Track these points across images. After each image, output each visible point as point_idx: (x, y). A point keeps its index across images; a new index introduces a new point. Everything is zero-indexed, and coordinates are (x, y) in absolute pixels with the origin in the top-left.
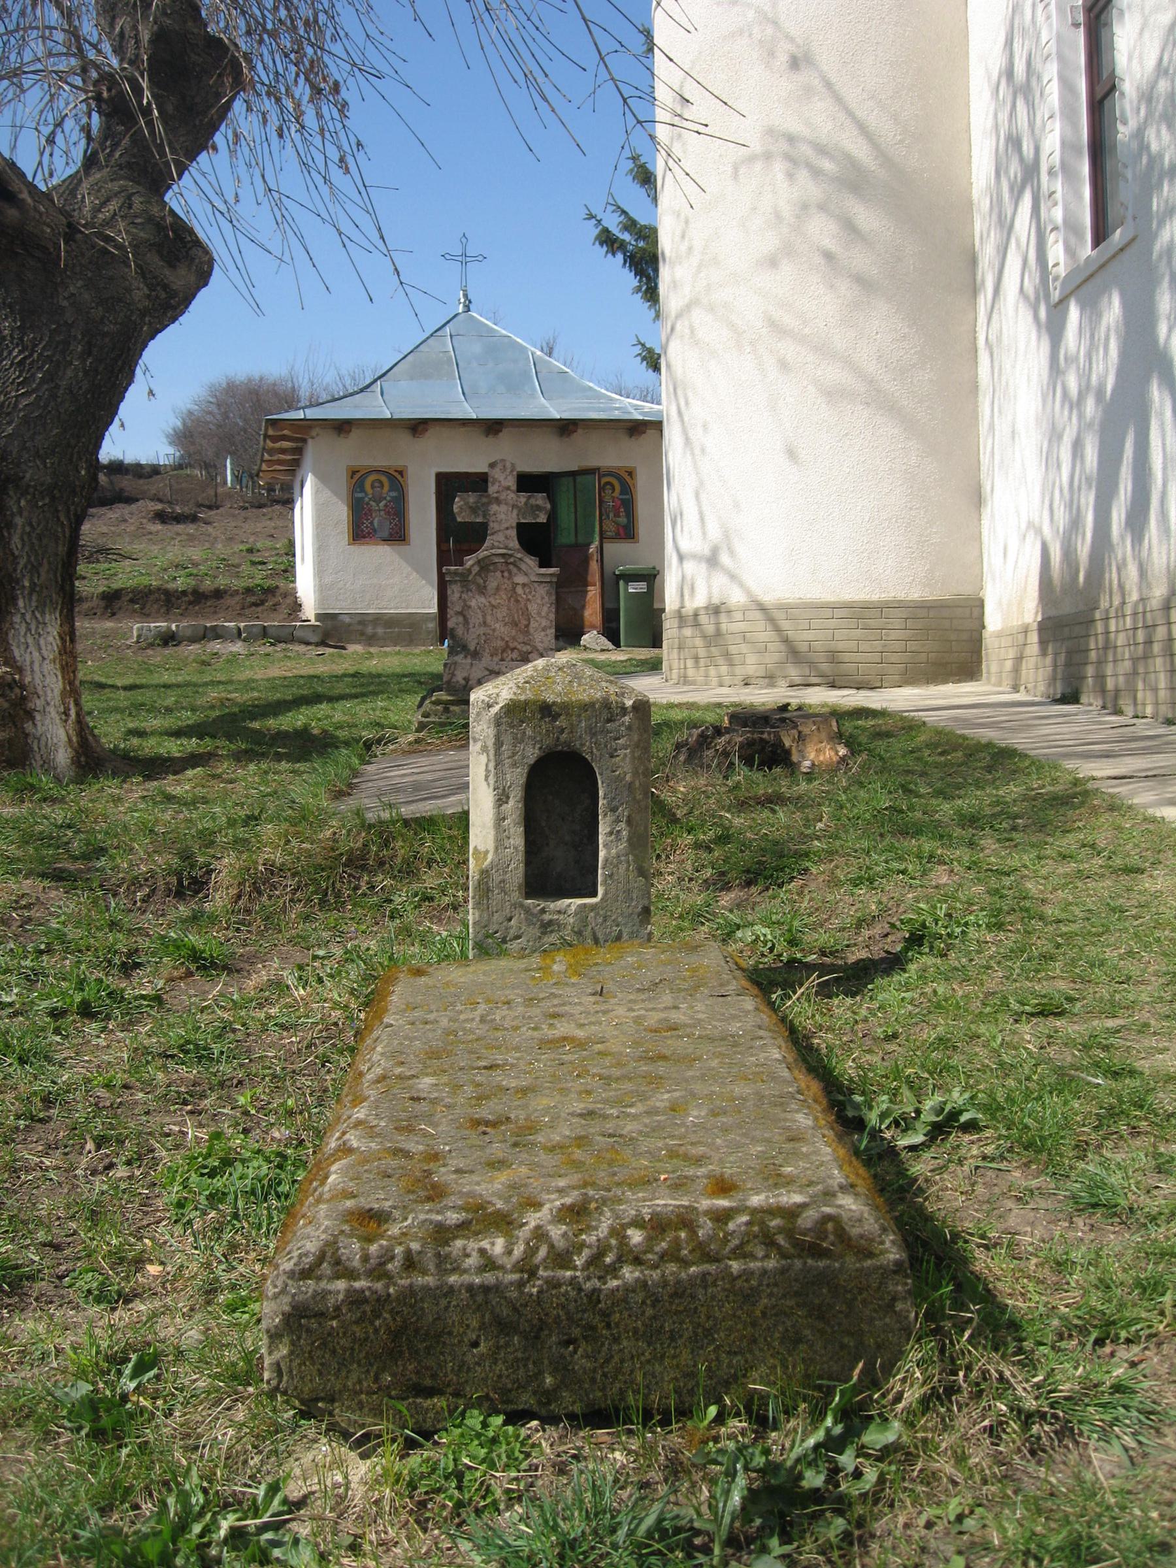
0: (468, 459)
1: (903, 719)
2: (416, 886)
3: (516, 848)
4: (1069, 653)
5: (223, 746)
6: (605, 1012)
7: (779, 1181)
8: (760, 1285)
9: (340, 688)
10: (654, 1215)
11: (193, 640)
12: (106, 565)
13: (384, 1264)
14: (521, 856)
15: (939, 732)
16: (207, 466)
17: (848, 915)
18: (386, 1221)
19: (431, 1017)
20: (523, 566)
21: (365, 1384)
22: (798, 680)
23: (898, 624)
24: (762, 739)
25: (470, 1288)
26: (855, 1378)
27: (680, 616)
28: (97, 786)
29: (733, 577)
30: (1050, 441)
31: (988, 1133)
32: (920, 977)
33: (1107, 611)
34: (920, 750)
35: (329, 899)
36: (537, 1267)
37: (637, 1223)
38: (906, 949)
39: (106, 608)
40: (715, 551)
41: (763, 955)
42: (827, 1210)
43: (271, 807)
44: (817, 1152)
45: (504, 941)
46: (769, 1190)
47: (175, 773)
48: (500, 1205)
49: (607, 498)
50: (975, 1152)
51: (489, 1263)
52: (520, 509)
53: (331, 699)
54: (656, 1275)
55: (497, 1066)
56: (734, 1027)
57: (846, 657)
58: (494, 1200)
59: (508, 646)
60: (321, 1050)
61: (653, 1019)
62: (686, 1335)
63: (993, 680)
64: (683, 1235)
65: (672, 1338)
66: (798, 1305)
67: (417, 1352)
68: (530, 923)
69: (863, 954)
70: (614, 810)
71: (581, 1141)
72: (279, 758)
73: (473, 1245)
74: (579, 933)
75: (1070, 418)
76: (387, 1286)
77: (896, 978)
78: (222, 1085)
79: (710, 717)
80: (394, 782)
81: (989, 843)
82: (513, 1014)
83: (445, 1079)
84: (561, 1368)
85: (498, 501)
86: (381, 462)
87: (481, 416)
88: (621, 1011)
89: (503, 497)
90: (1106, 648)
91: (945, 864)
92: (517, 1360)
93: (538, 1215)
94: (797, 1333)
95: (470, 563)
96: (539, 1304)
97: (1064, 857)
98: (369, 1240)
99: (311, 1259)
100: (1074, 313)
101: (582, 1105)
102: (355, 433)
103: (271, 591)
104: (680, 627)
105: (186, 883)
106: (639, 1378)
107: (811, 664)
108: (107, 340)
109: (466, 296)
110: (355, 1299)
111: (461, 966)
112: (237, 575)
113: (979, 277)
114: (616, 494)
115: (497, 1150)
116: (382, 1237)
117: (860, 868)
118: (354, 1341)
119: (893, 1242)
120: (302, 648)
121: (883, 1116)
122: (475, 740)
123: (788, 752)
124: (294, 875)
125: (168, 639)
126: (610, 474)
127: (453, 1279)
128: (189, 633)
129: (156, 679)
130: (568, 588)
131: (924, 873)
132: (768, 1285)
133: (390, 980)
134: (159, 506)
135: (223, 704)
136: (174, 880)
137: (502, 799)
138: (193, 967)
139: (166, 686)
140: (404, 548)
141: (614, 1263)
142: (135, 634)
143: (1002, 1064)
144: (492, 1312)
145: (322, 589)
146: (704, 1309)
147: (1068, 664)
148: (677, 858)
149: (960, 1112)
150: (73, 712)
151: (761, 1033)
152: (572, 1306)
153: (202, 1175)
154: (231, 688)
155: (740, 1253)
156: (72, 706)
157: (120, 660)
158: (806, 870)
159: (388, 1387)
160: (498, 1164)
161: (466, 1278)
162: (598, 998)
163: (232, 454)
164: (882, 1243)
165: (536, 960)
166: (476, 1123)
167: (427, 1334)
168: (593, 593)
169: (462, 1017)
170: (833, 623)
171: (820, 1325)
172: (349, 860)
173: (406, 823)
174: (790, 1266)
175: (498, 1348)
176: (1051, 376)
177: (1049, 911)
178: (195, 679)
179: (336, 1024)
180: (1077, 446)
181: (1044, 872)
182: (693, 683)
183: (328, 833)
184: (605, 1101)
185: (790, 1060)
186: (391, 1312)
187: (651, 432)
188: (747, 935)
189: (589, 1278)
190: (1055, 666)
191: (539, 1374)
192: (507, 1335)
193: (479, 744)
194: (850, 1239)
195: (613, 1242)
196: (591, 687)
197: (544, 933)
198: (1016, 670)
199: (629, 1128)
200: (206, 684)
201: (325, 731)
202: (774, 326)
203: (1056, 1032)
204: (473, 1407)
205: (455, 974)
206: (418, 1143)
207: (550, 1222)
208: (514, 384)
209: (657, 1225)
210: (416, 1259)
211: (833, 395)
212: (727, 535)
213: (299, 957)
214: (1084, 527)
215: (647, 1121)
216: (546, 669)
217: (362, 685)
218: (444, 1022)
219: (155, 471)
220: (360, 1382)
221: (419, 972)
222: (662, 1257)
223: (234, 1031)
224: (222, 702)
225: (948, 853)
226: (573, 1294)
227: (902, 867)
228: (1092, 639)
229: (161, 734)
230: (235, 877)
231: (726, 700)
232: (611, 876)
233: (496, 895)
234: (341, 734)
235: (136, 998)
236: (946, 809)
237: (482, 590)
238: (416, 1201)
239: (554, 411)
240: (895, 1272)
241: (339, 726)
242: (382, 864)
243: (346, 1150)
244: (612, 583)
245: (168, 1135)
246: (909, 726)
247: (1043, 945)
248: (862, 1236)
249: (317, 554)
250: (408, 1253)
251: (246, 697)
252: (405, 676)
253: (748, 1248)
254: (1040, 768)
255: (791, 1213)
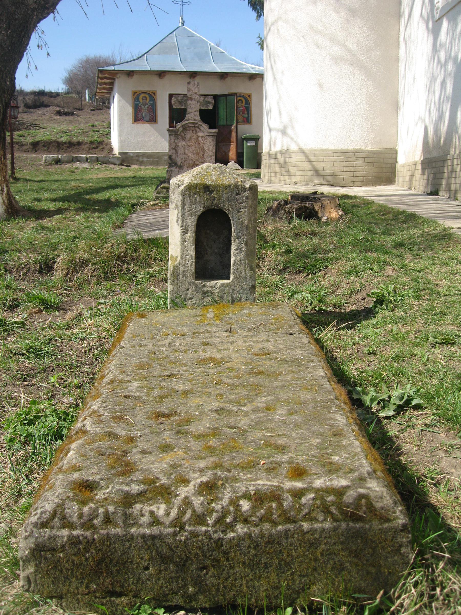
0: (180, 88)
1: (363, 199)
2: (148, 270)
3: (191, 256)
4: (435, 174)
5: (73, 205)
6: (232, 342)
7: (332, 469)
8: (320, 537)
9: (128, 183)
10: (257, 491)
11: (68, 162)
12: (33, 131)
13: (92, 519)
14: (193, 259)
15: (381, 206)
16: (78, 93)
17: (346, 288)
18: (96, 488)
19: (143, 343)
20: (202, 129)
21: (81, 589)
22: (317, 183)
23: (361, 160)
24: (305, 207)
25: (144, 536)
26: (378, 600)
27: (269, 155)
28: (15, 222)
29: (292, 139)
30: (431, 81)
31: (426, 411)
32: (383, 322)
33: (453, 156)
34: (373, 213)
35: (108, 276)
36: (185, 524)
37: (247, 496)
38: (375, 307)
39: (33, 149)
40: (285, 128)
41: (307, 306)
42: (362, 491)
43: (85, 233)
44: (351, 445)
45: (185, 300)
46: (326, 475)
47: (50, 217)
48: (164, 480)
49: (240, 106)
50: (421, 422)
51: (155, 521)
52: (201, 103)
53: (122, 187)
54: (257, 530)
55: (174, 375)
56: (298, 354)
57: (339, 173)
58: (161, 476)
59: (194, 164)
60: (96, 351)
61: (256, 348)
62: (274, 565)
63: (400, 184)
64: (274, 505)
65: (266, 567)
66: (342, 549)
67: (111, 573)
68: (197, 292)
69: (353, 308)
70: (239, 238)
71: (215, 432)
72: (95, 211)
73: (146, 508)
74: (222, 297)
75: (441, 71)
76: (93, 534)
77: (371, 321)
78: (44, 370)
79: (281, 197)
80: (140, 223)
81: (408, 256)
82: (186, 342)
83: (145, 384)
84: (199, 583)
85: (191, 99)
86: (146, 89)
87: (188, 70)
88: (240, 342)
89: (193, 97)
90: (452, 172)
91: (390, 265)
92: (171, 578)
93: (186, 489)
94: (341, 565)
95: (179, 126)
96: (185, 546)
97: (444, 264)
98: (84, 503)
99: (46, 516)
100: (445, 23)
101: (217, 404)
102: (135, 77)
103: (101, 143)
104: (269, 159)
105: (43, 267)
106: (245, 589)
107: (323, 176)
108: (17, 22)
109: (182, 19)
110: (74, 542)
111: (163, 312)
112: (87, 136)
113: (402, 10)
114: (243, 104)
115: (167, 437)
116: (92, 500)
117: (352, 267)
118: (74, 564)
119: (401, 511)
120: (113, 166)
121: (372, 400)
122: (172, 203)
123: (317, 213)
124: (92, 264)
125: (58, 162)
126: (241, 96)
127: (133, 530)
128: (66, 159)
129: (52, 178)
130: (222, 141)
131: (381, 270)
132: (325, 538)
133: (128, 319)
134: (58, 109)
135: (77, 189)
136: (38, 266)
137: (184, 231)
138: (42, 308)
139: (56, 181)
140: (155, 125)
141: (232, 522)
142: (44, 159)
143: (428, 370)
144: (157, 551)
145: (121, 142)
146: (285, 551)
147: (434, 179)
148: (267, 259)
149: (412, 399)
150: (5, 190)
151: (313, 358)
152: (206, 548)
153: (24, 424)
154: (81, 182)
155: (308, 517)
156: (5, 187)
157: (38, 170)
158: (327, 267)
159: (94, 592)
160: (166, 448)
161: (142, 530)
162: (228, 334)
163: (88, 87)
164: (394, 512)
165: (199, 311)
166: (158, 415)
167: (117, 562)
168: (233, 145)
169: (159, 343)
170: (333, 159)
171: (355, 560)
172: (118, 257)
173: (145, 241)
174: (339, 526)
175: (160, 571)
176: (432, 53)
177: (441, 290)
178: (67, 178)
179: (104, 338)
180: (443, 83)
181: (436, 271)
182: (274, 183)
183: (109, 245)
184: (230, 402)
185: (329, 375)
186: (95, 549)
187: (258, 79)
188: (299, 297)
189: (216, 532)
190: (428, 179)
191: (185, 586)
192: (166, 563)
193: (174, 204)
194: (375, 510)
195: (232, 509)
196: (229, 178)
197: (204, 297)
198: (411, 181)
199: (242, 422)
200: (71, 180)
201: (117, 200)
202: (312, 28)
203: (453, 354)
204: (145, 603)
205: (160, 318)
206: (123, 429)
207: (194, 495)
208: (202, 57)
209: (259, 498)
210: (111, 517)
211: (337, 60)
212: (291, 121)
213: (93, 303)
214: (444, 119)
215: (253, 417)
216: (207, 168)
217: (136, 181)
218: (150, 346)
219: (57, 95)
220: (77, 588)
221: (142, 316)
222: (261, 519)
223: (56, 341)
224: (77, 187)
225: (392, 261)
226: (206, 540)
227: (372, 267)
228: (446, 168)
229: (48, 200)
230: (66, 265)
231: (288, 190)
232: (237, 270)
233: (181, 278)
234: (123, 201)
235: (12, 323)
236: (388, 240)
237: (184, 139)
238: (114, 475)
239: (219, 69)
240: (402, 531)
241: (124, 198)
242: (133, 259)
243: (83, 432)
244: (241, 142)
245: (12, 398)
246: (368, 203)
247: (439, 307)
248: (382, 508)
249: (120, 129)
250: (107, 512)
251: (87, 185)
252: (154, 178)
253: (313, 515)
254: (428, 222)
255: (340, 493)
